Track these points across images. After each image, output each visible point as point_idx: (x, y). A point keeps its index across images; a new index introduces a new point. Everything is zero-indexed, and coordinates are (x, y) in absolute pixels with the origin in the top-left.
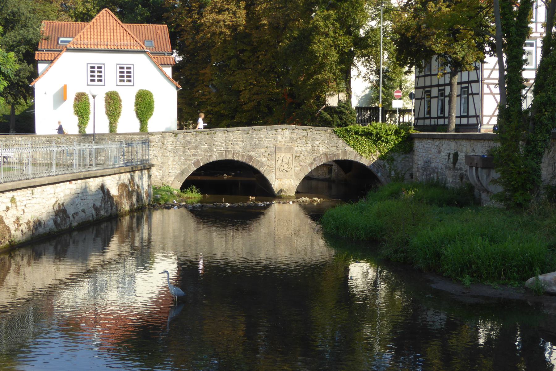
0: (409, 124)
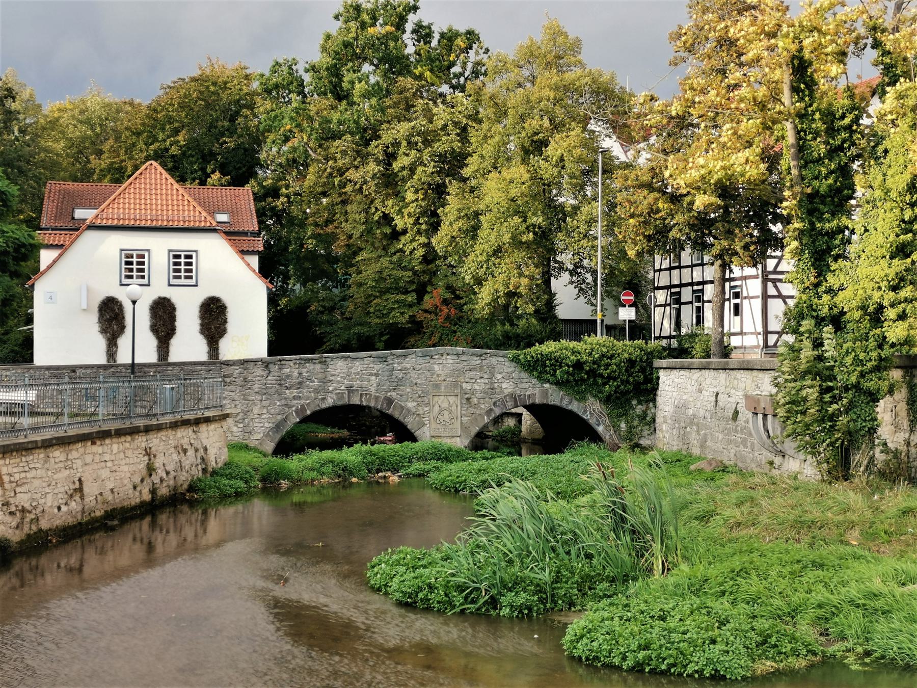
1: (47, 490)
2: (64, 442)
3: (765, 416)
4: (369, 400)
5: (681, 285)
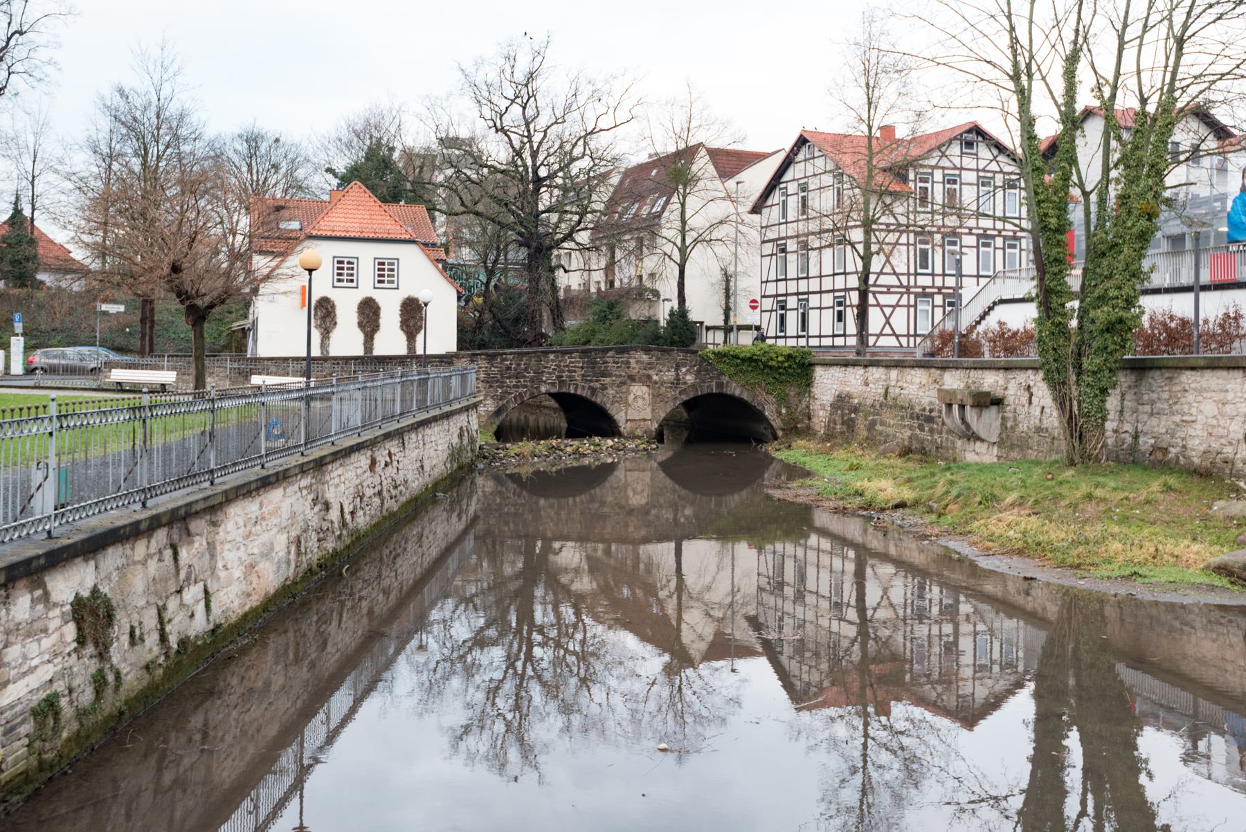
2: (733, 559)
3: (962, 407)
5: (786, 295)
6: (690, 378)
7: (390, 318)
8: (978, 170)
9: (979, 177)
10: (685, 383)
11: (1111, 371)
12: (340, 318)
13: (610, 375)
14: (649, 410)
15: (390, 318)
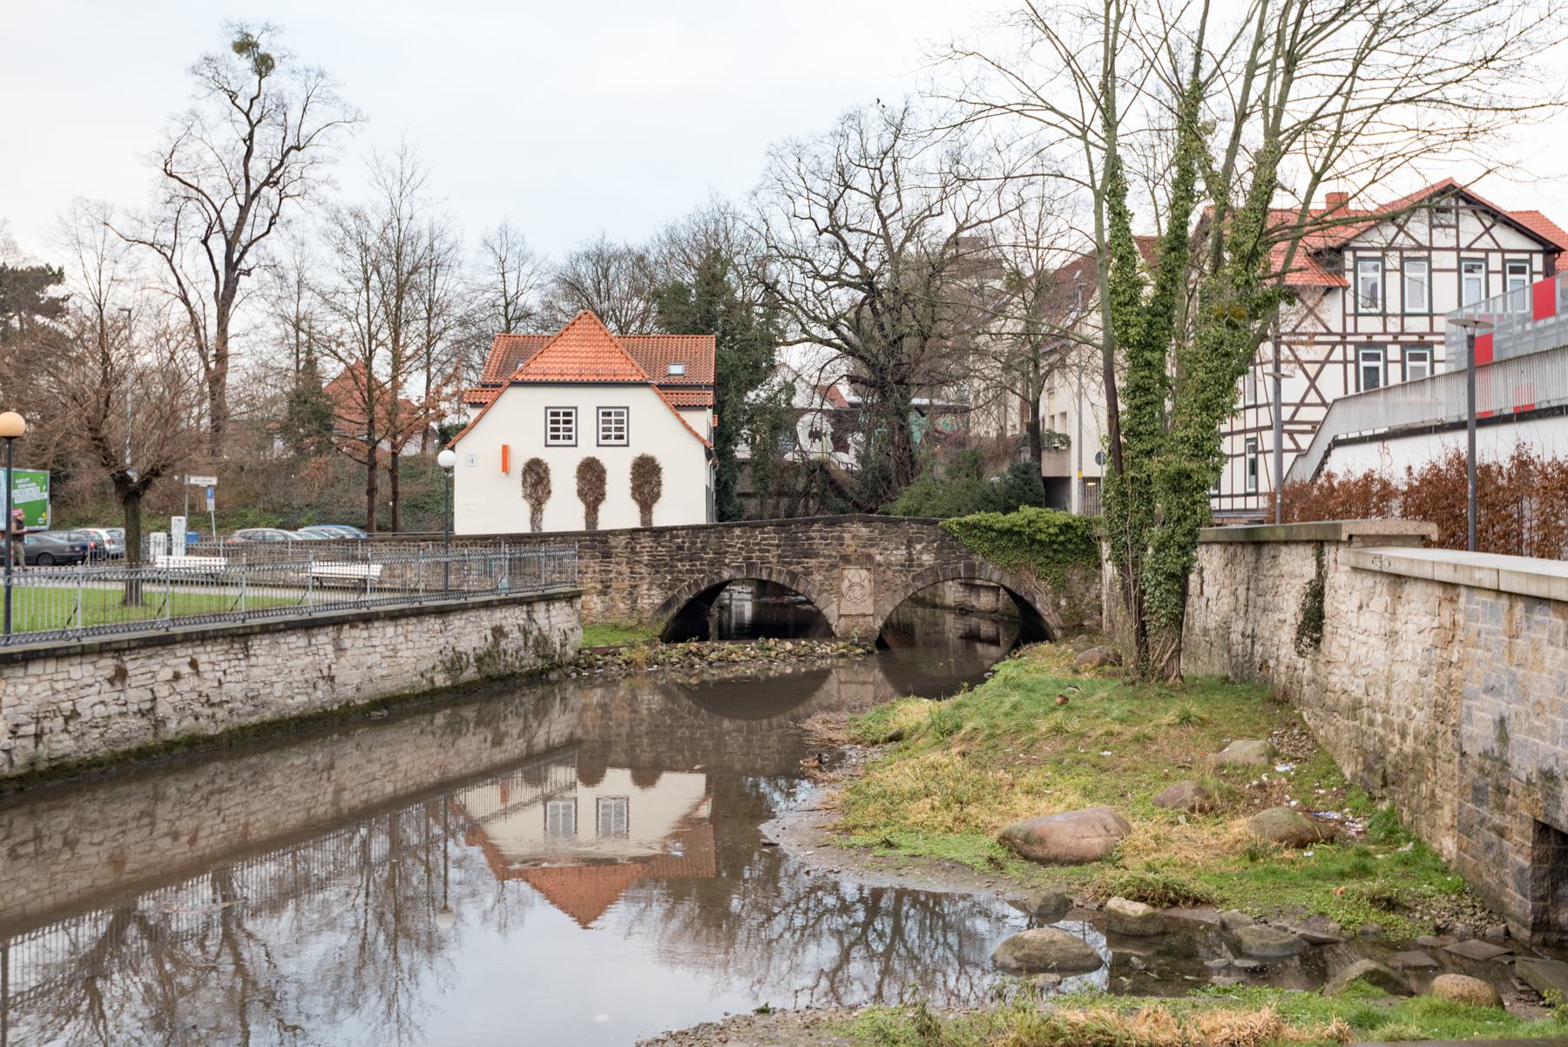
0: (1338, 771)
1: (275, 679)
4: (770, 574)
6: (927, 559)
7: (619, 483)
8: (1458, 249)
9: (1460, 260)
10: (921, 565)
11: (1181, 548)
12: (555, 486)
13: (816, 555)
14: (870, 602)
15: (619, 483)
